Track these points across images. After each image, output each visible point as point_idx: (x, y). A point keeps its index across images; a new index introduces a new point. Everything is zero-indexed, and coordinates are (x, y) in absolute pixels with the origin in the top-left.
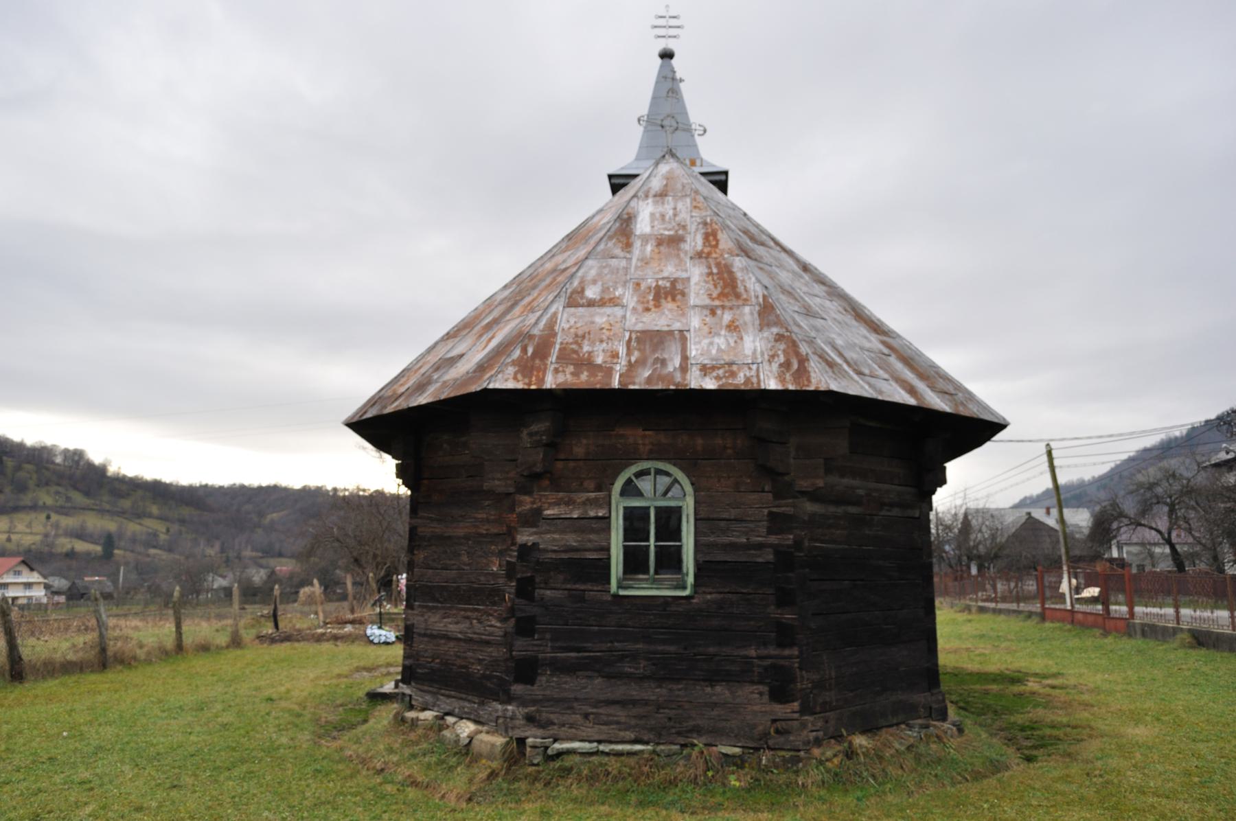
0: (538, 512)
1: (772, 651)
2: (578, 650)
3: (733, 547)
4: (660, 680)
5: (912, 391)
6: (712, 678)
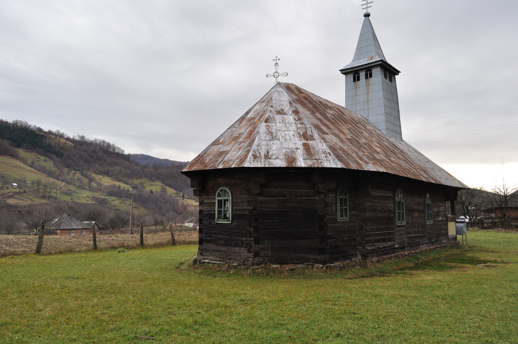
0: (203, 201)
1: (248, 239)
2: (211, 237)
3: (240, 210)
4: (226, 245)
5: (357, 163)
6: (236, 245)
